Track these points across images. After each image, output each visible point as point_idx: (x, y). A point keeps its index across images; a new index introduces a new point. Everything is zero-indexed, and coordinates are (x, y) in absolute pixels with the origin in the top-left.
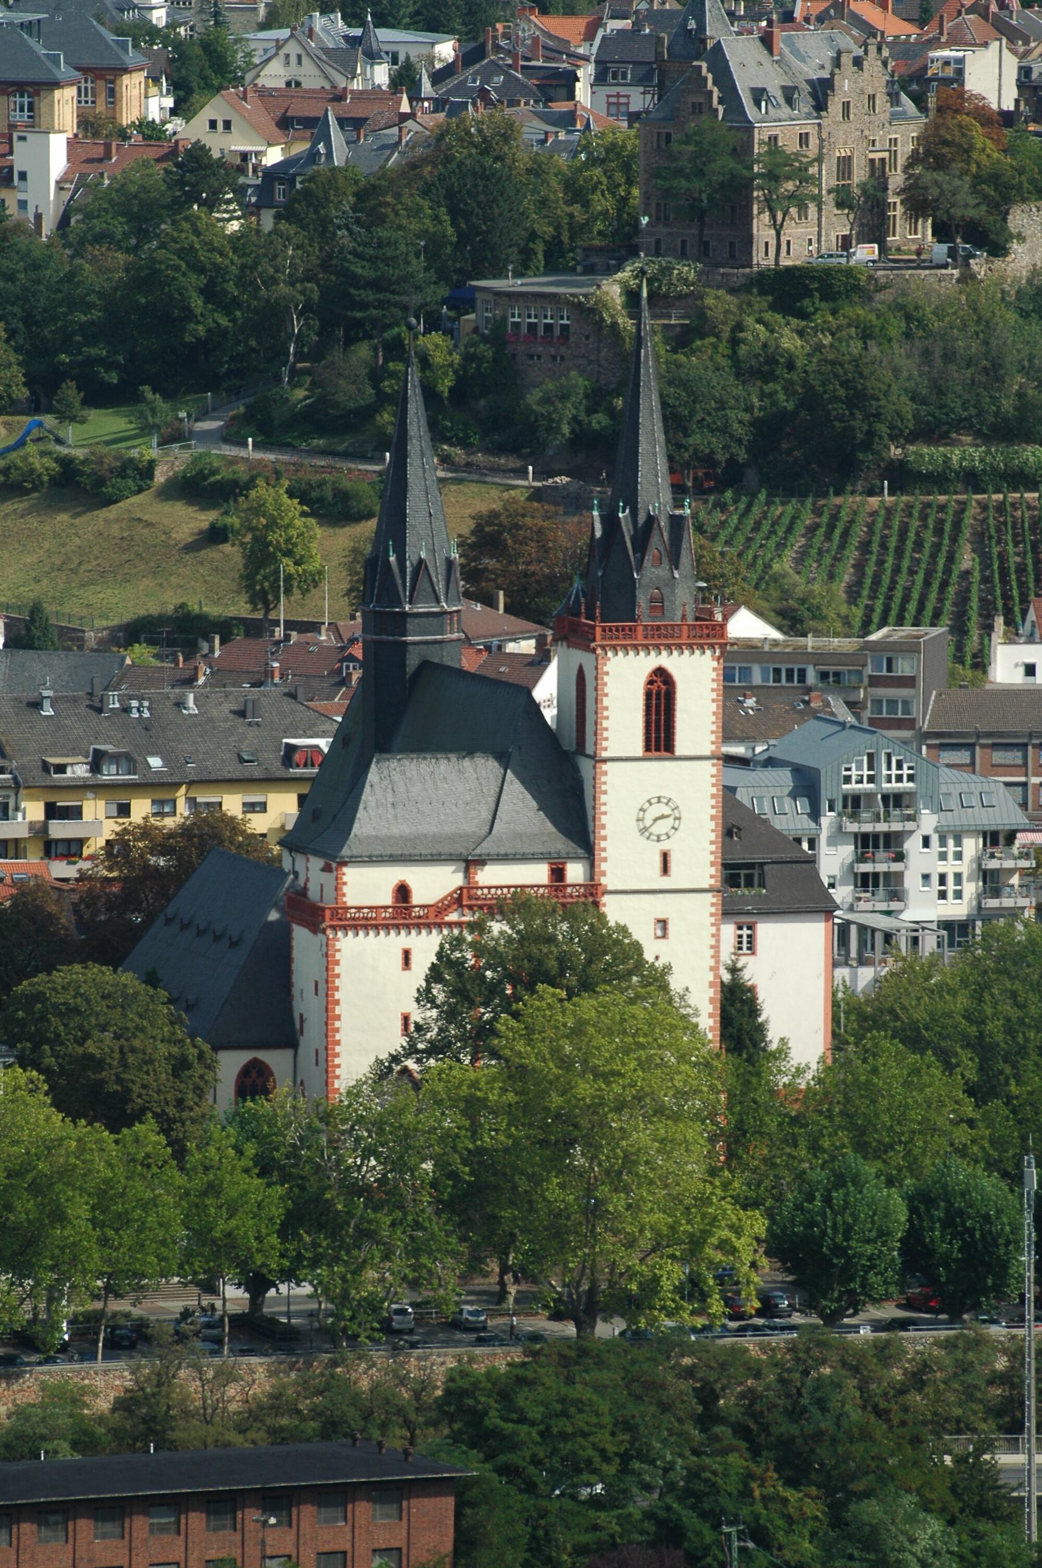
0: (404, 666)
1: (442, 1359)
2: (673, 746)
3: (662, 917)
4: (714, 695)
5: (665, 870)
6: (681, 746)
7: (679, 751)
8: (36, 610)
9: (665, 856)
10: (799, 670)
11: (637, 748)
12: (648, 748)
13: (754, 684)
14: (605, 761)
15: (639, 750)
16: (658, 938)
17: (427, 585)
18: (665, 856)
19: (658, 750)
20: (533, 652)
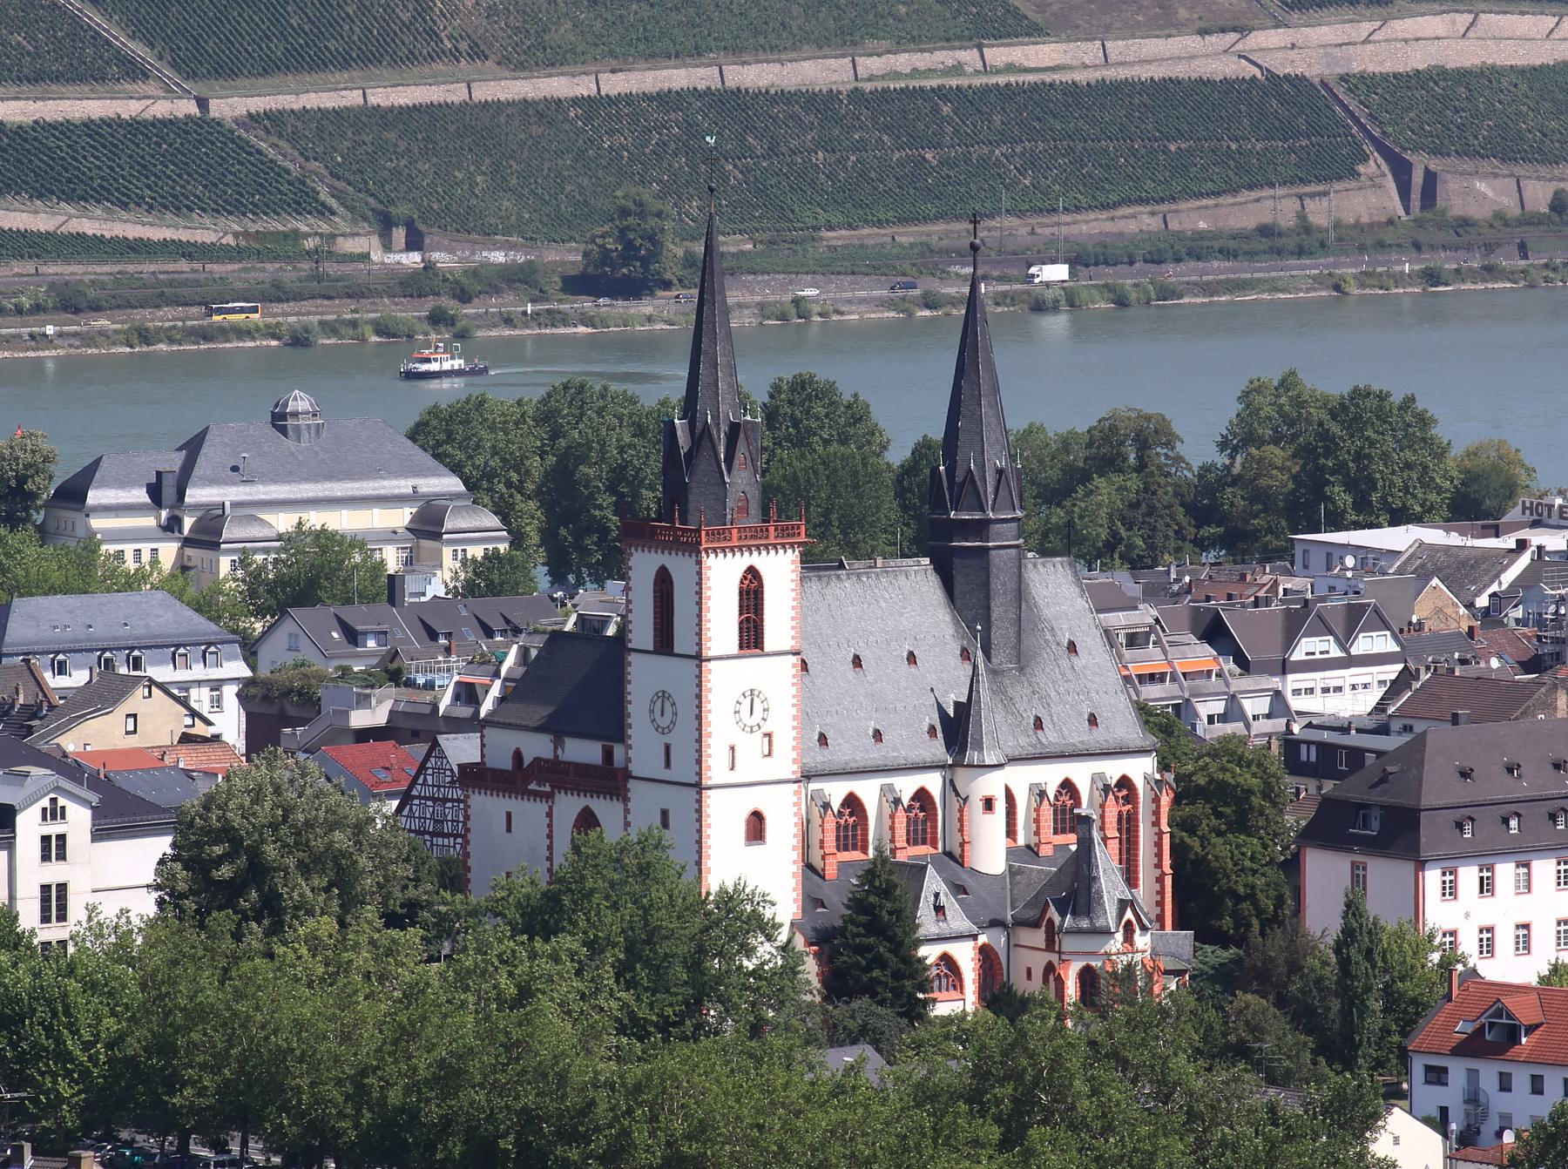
0: (550, 716)
1: (1201, 763)
2: (762, 643)
3: (1487, 923)
4: (629, 678)
5: (668, 764)
6: (769, 646)
7: (768, 647)
8: (1293, 373)
9: (668, 748)
10: (49, 921)
11: (734, 648)
12: (741, 647)
13: (177, 468)
14: (709, 660)
15: (735, 650)
16: (127, 733)
17: (1007, 493)
18: (668, 748)
19: (749, 648)
20: (145, 906)
